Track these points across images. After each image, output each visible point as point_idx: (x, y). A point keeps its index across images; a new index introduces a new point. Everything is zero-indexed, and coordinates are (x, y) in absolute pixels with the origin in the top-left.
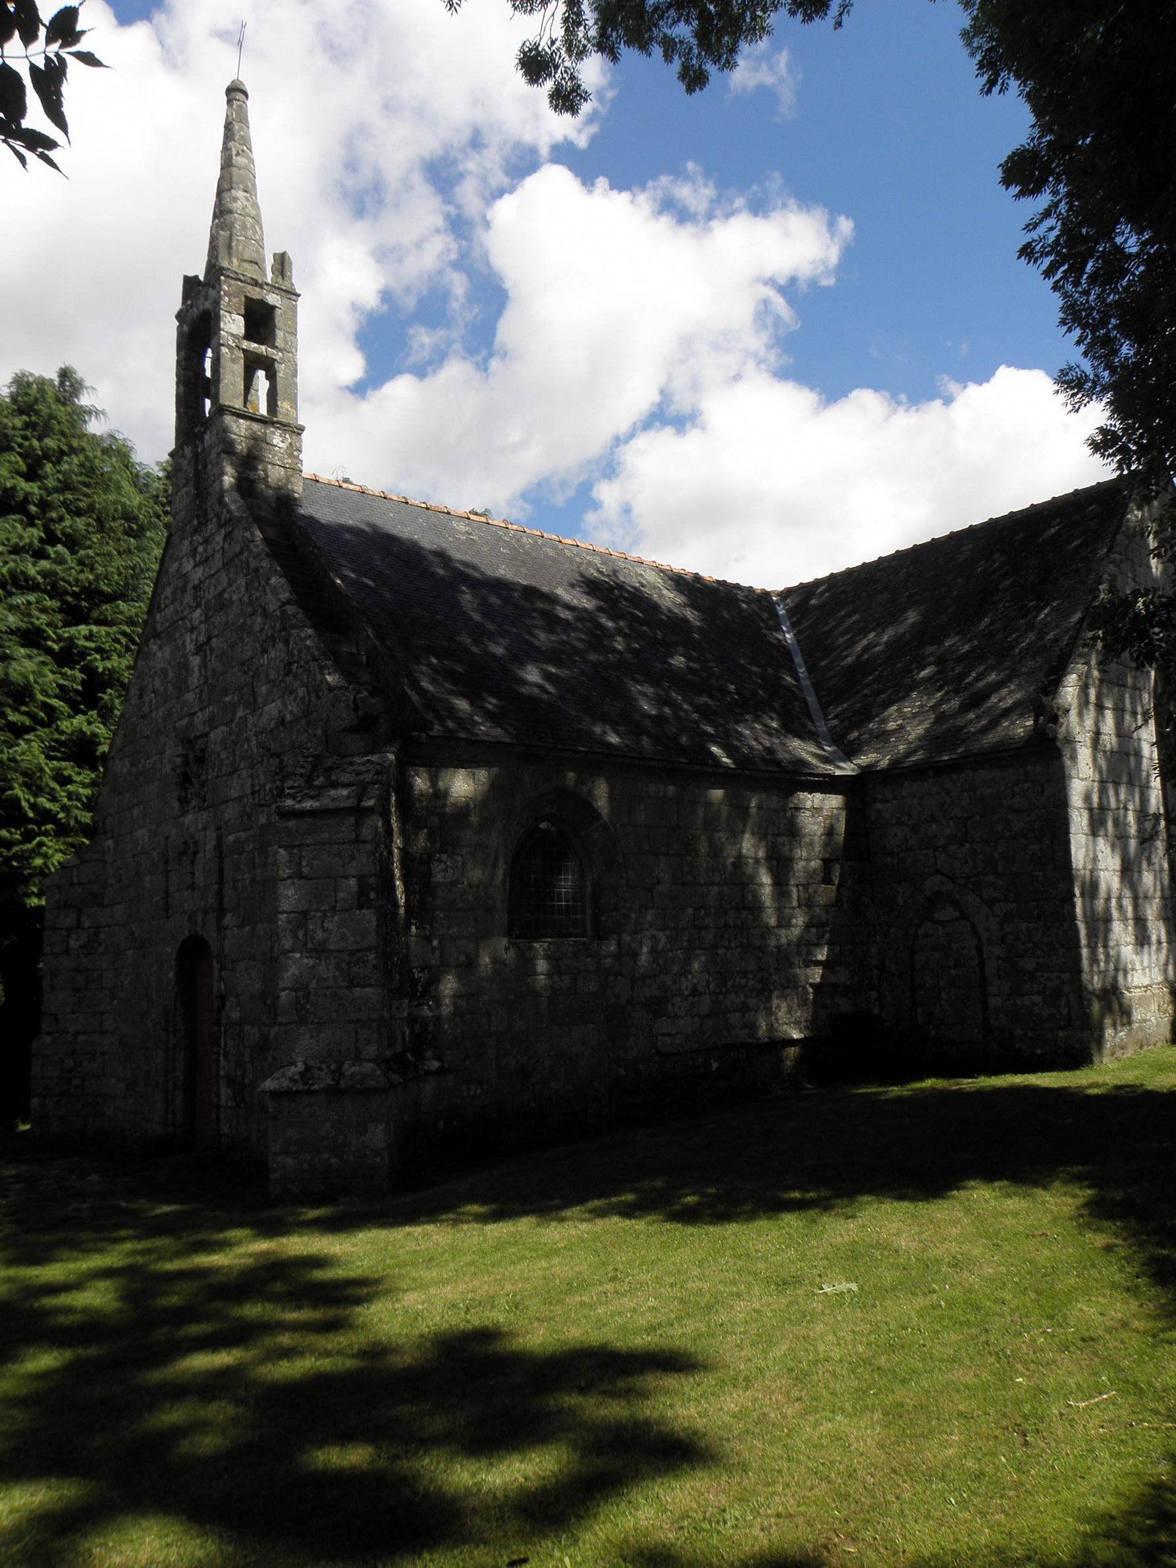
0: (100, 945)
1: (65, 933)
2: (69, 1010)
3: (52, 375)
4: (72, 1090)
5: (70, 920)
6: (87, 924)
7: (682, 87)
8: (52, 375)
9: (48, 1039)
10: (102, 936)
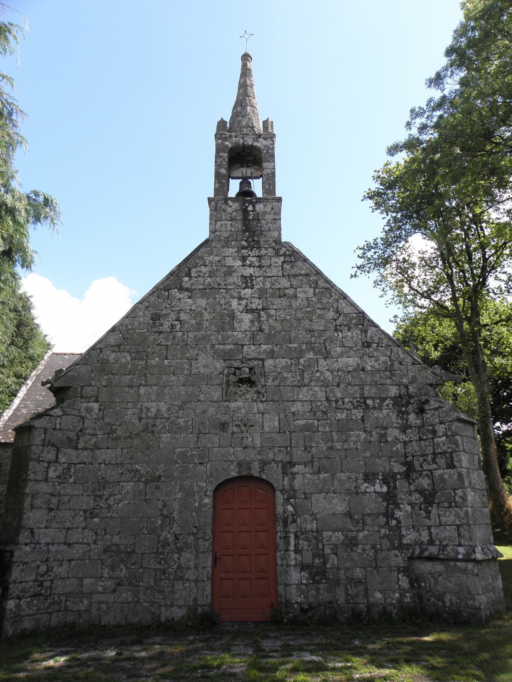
0: (71, 477)
1: (46, 465)
2: (44, 525)
3: (278, 195)
4: (43, 592)
5: (50, 456)
6: (63, 460)
7: (270, 120)
8: (278, 195)
9: (28, 549)
10: (73, 470)
